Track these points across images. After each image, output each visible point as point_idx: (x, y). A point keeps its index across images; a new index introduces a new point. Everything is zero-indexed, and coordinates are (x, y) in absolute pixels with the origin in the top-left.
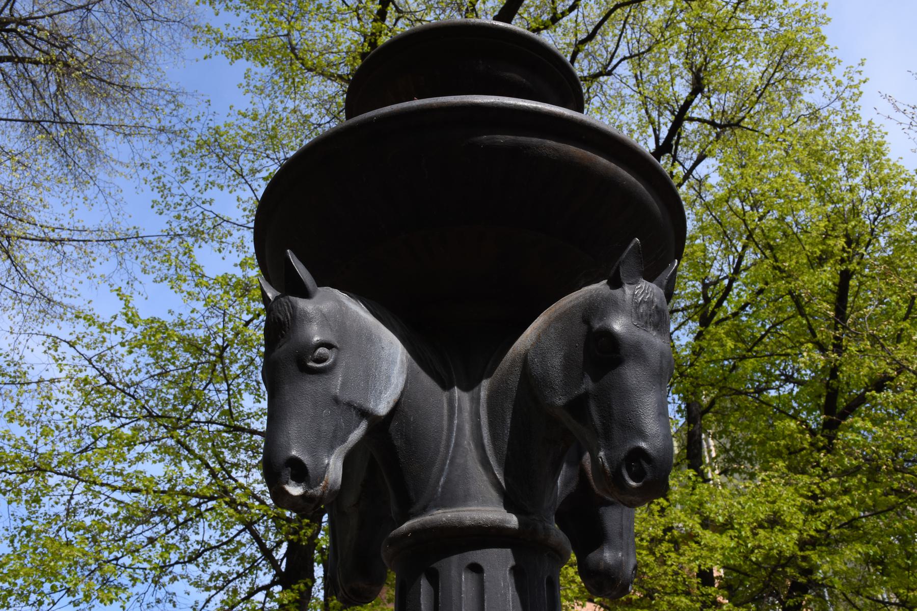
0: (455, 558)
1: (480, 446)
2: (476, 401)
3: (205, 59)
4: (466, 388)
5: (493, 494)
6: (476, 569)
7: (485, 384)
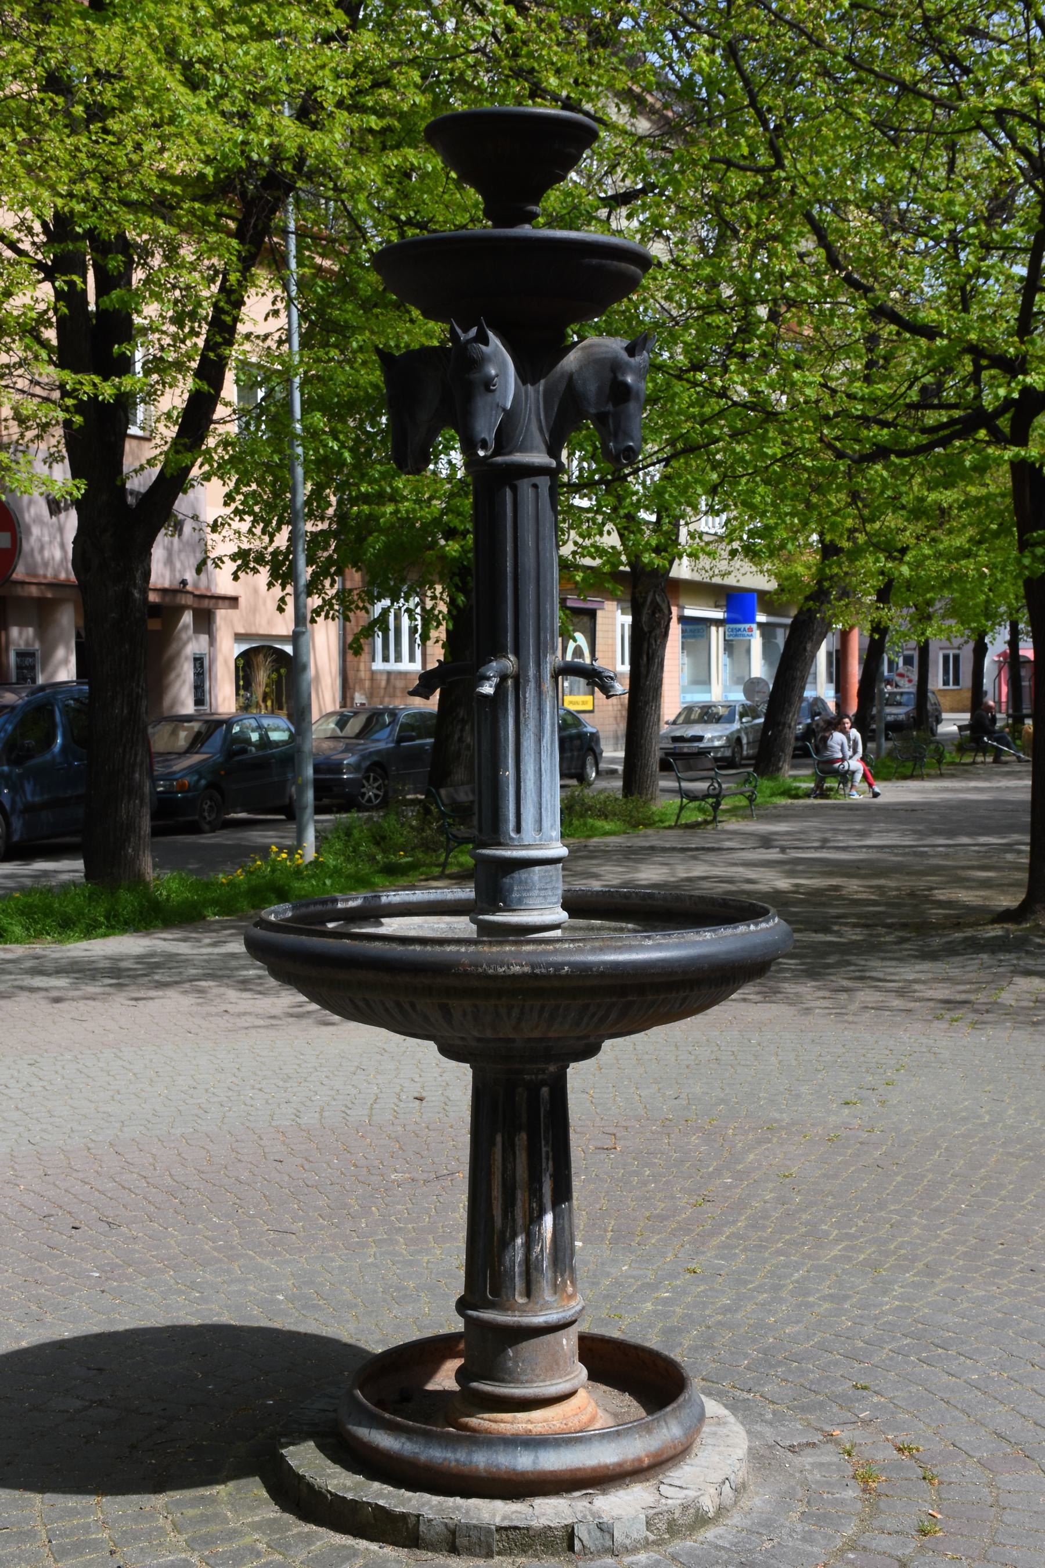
0: (526, 480)
1: (539, 420)
2: (537, 392)
3: (266, 319)
4: (533, 384)
5: (543, 447)
6: (535, 486)
7: (542, 382)
